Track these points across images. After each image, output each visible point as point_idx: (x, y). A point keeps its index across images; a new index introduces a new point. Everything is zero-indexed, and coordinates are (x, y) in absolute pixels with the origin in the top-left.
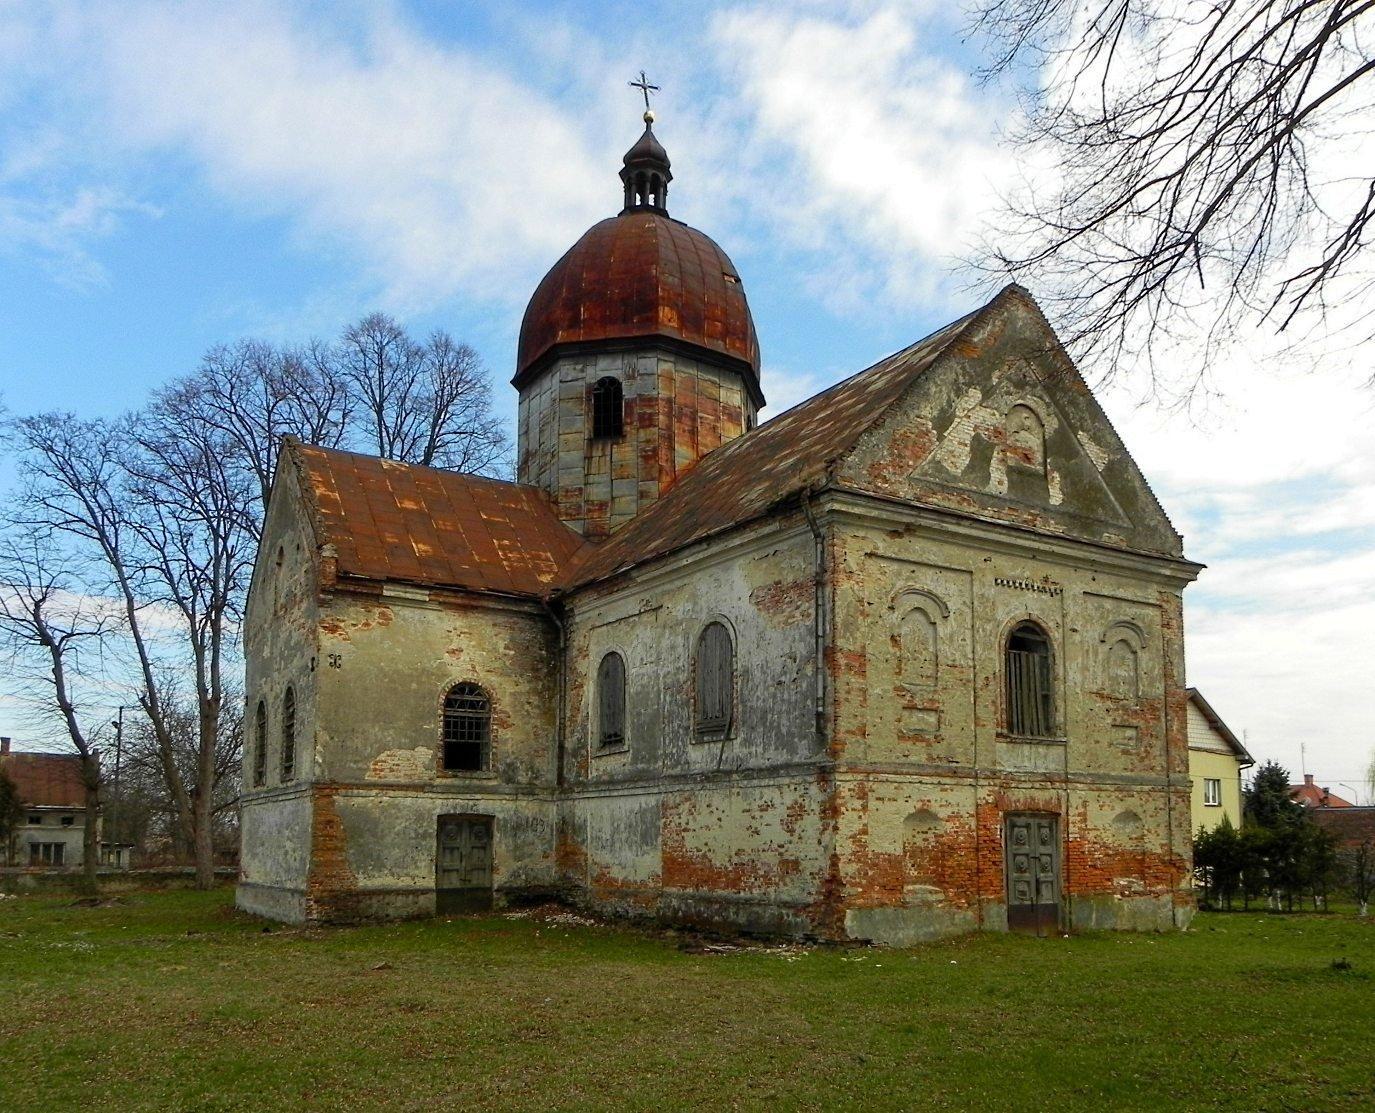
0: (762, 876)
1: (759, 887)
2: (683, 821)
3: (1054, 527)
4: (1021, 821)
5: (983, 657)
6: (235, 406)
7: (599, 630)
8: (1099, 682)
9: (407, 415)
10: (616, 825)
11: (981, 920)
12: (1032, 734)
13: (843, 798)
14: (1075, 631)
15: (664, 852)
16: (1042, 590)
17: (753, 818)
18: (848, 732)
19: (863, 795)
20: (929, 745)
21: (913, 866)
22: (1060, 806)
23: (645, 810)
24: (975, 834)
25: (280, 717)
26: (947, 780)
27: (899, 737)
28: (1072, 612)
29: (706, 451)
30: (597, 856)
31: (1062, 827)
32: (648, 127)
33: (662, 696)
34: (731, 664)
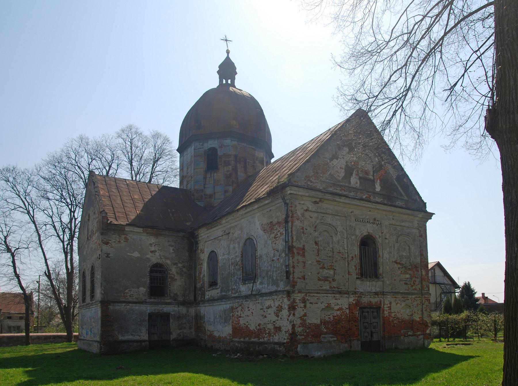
0: (267, 333)
1: (267, 337)
2: (239, 314)
3: (377, 199)
4: (365, 310)
5: (351, 249)
6: (77, 163)
7: (208, 242)
8: (396, 257)
9: (142, 165)
10: (215, 316)
11: (351, 347)
12: (370, 278)
13: (297, 303)
14: (386, 239)
15: (232, 325)
16: (374, 223)
17: (264, 312)
18: (298, 278)
19: (304, 301)
20: (330, 282)
21: (325, 328)
22: (381, 304)
23: (225, 310)
24: (348, 315)
25: (90, 277)
26: (337, 295)
27: (318, 280)
28: (385, 232)
29: (250, 174)
30: (209, 328)
31: (381, 312)
32: (228, 55)
33: (231, 267)
34: (255, 254)
